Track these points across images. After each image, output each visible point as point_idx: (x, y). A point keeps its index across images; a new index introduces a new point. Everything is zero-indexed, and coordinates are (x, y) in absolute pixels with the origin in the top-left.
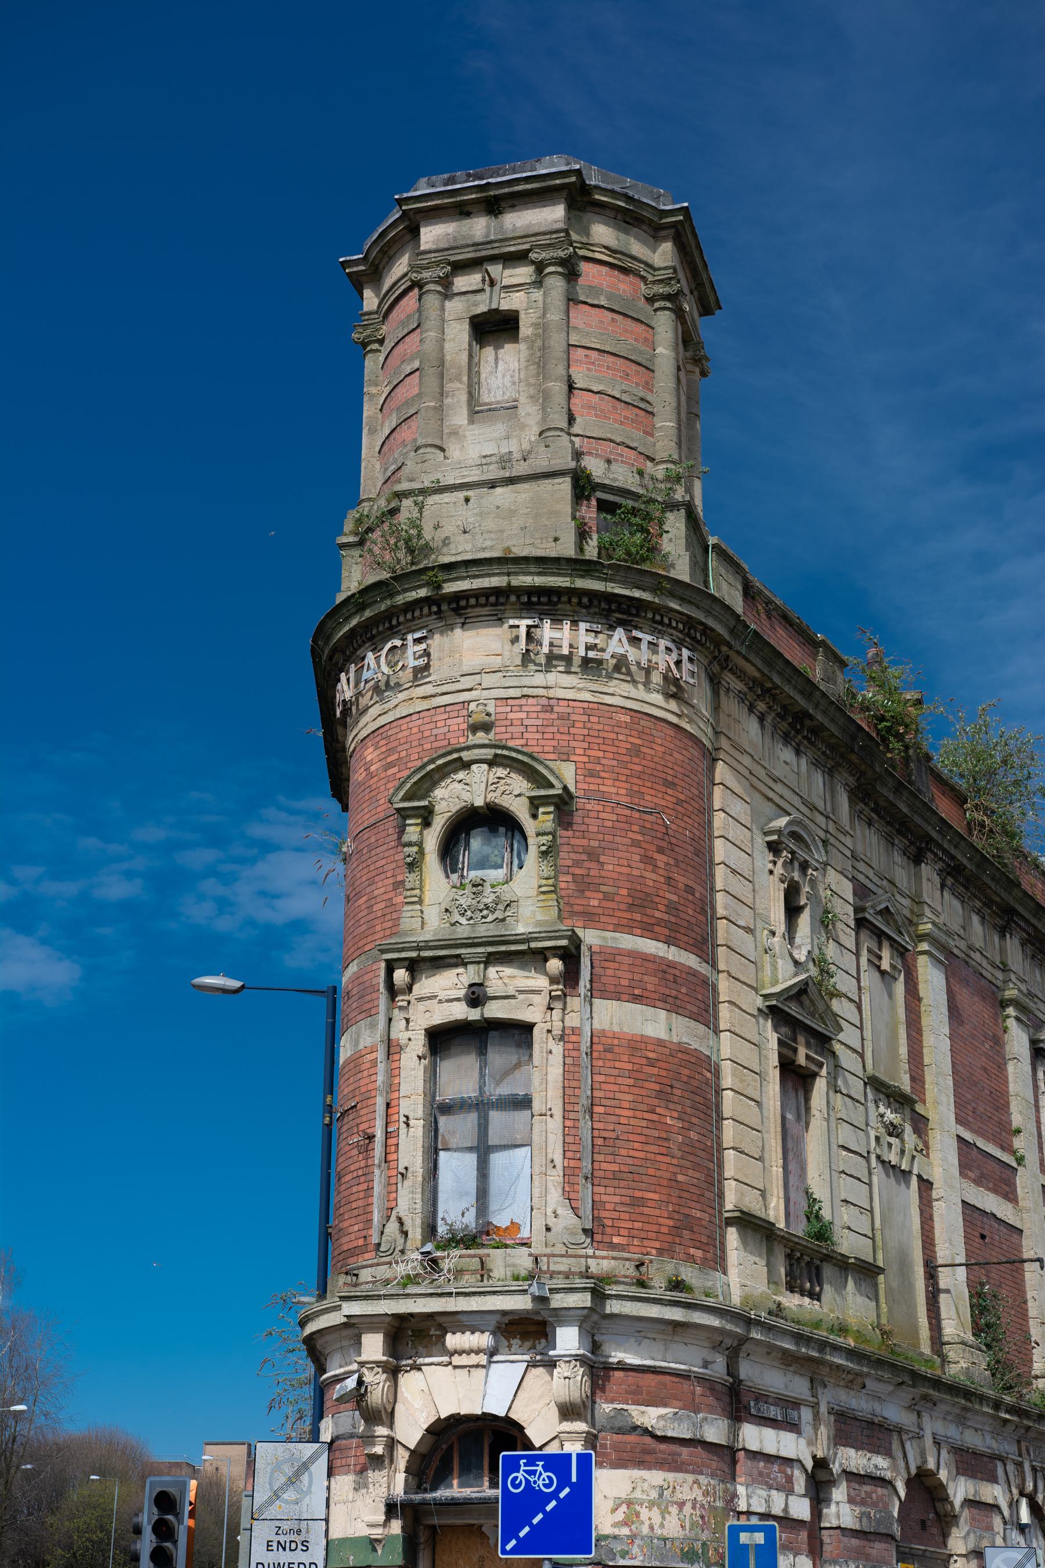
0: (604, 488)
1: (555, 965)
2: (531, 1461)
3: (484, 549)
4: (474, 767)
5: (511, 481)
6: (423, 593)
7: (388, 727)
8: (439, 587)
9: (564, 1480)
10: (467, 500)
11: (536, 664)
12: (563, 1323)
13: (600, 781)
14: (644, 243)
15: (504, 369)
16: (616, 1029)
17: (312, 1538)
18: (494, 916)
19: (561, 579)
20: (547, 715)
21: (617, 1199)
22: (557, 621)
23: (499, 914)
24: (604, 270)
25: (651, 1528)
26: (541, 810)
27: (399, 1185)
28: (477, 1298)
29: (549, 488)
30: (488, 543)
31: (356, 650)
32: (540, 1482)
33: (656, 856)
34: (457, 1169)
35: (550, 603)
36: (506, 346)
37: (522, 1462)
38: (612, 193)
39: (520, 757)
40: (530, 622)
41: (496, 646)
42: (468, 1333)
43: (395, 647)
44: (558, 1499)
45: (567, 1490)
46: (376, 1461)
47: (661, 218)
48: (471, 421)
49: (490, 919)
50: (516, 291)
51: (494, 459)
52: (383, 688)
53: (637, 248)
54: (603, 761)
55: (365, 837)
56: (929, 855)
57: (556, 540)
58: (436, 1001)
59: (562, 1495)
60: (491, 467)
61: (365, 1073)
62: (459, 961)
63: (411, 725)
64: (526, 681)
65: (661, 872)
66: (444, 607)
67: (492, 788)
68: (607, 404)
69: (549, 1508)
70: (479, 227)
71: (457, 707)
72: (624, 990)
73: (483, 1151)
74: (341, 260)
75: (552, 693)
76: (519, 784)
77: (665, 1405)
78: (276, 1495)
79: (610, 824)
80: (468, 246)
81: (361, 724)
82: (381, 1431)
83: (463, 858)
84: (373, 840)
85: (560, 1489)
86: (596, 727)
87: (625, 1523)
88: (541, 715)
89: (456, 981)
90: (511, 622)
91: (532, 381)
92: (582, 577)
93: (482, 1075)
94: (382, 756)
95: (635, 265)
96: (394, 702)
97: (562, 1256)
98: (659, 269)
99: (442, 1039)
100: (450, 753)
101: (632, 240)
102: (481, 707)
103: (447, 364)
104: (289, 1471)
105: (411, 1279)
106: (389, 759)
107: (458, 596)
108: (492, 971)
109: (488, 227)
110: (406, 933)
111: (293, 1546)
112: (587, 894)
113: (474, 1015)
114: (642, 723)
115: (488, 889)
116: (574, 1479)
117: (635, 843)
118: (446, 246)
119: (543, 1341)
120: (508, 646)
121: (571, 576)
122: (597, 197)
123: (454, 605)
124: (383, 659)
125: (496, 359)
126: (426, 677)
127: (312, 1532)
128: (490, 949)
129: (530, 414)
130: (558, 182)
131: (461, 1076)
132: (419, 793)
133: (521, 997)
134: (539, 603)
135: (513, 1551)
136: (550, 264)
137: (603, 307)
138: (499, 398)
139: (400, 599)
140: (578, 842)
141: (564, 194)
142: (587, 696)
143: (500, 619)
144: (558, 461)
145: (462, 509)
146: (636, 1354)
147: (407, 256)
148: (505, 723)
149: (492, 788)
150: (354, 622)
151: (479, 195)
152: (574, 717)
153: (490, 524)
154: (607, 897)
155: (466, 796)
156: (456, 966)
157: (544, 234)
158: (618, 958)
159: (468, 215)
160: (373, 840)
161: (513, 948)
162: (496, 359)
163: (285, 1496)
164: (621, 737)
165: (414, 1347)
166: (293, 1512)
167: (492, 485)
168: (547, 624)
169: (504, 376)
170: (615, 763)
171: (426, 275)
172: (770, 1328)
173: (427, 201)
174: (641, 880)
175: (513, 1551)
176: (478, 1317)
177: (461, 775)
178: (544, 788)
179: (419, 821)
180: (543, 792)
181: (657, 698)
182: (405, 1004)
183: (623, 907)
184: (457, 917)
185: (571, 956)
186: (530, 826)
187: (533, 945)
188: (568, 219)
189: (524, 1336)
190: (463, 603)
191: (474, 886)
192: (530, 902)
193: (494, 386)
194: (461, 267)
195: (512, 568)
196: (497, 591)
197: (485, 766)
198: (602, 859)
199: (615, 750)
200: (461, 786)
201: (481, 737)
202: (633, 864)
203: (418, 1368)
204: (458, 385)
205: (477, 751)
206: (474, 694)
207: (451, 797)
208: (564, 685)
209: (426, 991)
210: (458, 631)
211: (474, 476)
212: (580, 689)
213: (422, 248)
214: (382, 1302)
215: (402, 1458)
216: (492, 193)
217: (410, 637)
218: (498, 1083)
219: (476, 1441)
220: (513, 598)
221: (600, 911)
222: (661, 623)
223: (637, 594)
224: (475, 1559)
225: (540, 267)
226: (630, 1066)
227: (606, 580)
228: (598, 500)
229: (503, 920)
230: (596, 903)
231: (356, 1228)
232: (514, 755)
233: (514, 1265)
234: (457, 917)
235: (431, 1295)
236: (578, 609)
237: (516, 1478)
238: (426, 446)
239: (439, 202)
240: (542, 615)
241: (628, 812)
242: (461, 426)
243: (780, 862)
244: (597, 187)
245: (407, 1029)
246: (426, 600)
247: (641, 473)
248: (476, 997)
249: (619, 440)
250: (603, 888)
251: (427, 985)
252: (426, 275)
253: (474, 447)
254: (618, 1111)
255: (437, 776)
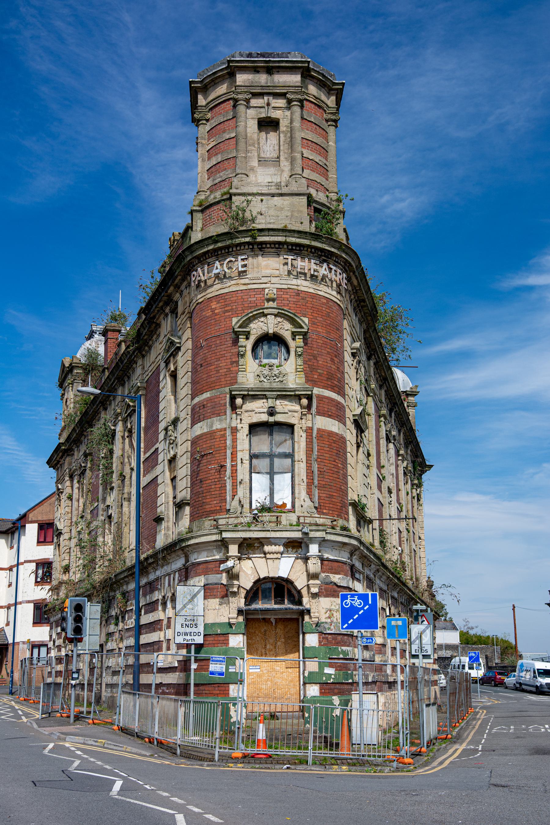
0: (316, 202)
1: (305, 402)
2: (353, 596)
3: (270, 223)
4: (268, 316)
5: (281, 195)
6: (248, 239)
7: (225, 295)
8: (256, 239)
9: (366, 603)
10: (262, 200)
11: (293, 275)
12: (312, 543)
13: (317, 326)
14: (325, 95)
15: (270, 143)
16: (323, 428)
17: (199, 623)
18: (279, 380)
19: (306, 241)
20: (297, 297)
21: (325, 495)
22: (303, 258)
23: (280, 379)
24: (313, 106)
25: (337, 619)
26: (297, 337)
27: (238, 486)
28: (279, 532)
29: (298, 200)
30: (272, 221)
31: (206, 259)
32: (357, 604)
33: (335, 358)
34: (260, 482)
35: (300, 250)
36: (271, 133)
37: (349, 596)
38: (318, 72)
39: (289, 314)
40: (292, 257)
41: (277, 266)
42: (273, 546)
43: (231, 261)
44: (364, 610)
45: (367, 607)
46: (234, 594)
47: (333, 86)
48: (259, 165)
49: (277, 380)
50: (277, 109)
51: (273, 184)
52: (223, 277)
53: (323, 97)
54: (318, 318)
55: (214, 340)
56: (373, 357)
57: (302, 223)
58: (254, 412)
59: (365, 608)
60: (272, 187)
61: (218, 440)
62: (265, 397)
63: (237, 295)
64: (290, 282)
65: (336, 365)
66: (255, 247)
67: (276, 326)
68: (315, 165)
69: (360, 613)
70: (262, 78)
71: (260, 290)
72: (326, 412)
73: (272, 474)
74: (190, 80)
75: (299, 288)
76: (287, 325)
77: (340, 574)
78: (185, 606)
79: (320, 344)
80: (258, 86)
81: (208, 291)
82: (236, 582)
83: (261, 353)
84: (218, 342)
85: (364, 606)
86: (315, 304)
87: (329, 617)
88: (295, 297)
89: (263, 405)
90: (285, 257)
91: (286, 151)
92: (314, 241)
93: (271, 444)
94: (222, 307)
95: (323, 105)
96: (229, 284)
97: (306, 517)
98: (331, 108)
99: (254, 428)
100: (259, 310)
101: (322, 94)
102: (271, 292)
103: (248, 138)
104: (189, 598)
105: (249, 524)
106: (226, 309)
107: (262, 243)
108: (278, 402)
109: (267, 79)
110: (242, 383)
111: (192, 626)
112: (313, 373)
113: (271, 419)
114: (330, 303)
115: (275, 368)
116: (370, 602)
117: (328, 353)
118: (249, 85)
119: (300, 549)
120: (282, 266)
121: (310, 240)
122: (312, 73)
123: (260, 247)
124: (225, 265)
125: (267, 138)
126: (245, 275)
127: (199, 620)
128: (279, 393)
129: (285, 164)
130: (300, 65)
131: (262, 443)
132: (244, 325)
133: (290, 413)
134: (296, 250)
135: (346, 628)
136: (295, 101)
137: (312, 122)
138: (268, 156)
139: (238, 241)
140: (309, 351)
141: (301, 70)
142: (311, 291)
143: (278, 254)
144: (302, 189)
145: (259, 204)
146: (331, 555)
147: (226, 84)
148: (281, 299)
149: (276, 326)
150: (211, 247)
151: (265, 65)
152: (308, 299)
153: (272, 212)
154: (320, 375)
155: (265, 328)
156: (263, 399)
157: (292, 87)
158: (324, 400)
159: (258, 72)
160: (218, 342)
161: (288, 393)
162: (267, 138)
163: (188, 607)
164: (324, 309)
165: (247, 550)
166: (191, 613)
167: (273, 195)
168: (299, 259)
169: (270, 146)
170: (321, 319)
171: (240, 96)
172: (368, 548)
173: (241, 63)
174: (330, 368)
175: (346, 628)
176: (278, 540)
177: (262, 319)
178: (297, 328)
179: (245, 337)
180: (299, 330)
181: (334, 293)
182: (240, 413)
183: (325, 379)
184: (262, 379)
185: (310, 398)
186: (292, 344)
187: (297, 393)
188: (302, 81)
189: (293, 547)
190: (264, 246)
191: (270, 366)
192: (292, 375)
193: (266, 150)
194: (256, 95)
195: (288, 234)
196: (279, 243)
197: (273, 317)
198: (318, 359)
199: (322, 314)
200: (262, 324)
201: (271, 304)
202: (328, 362)
203: (250, 559)
204: (253, 148)
205: (271, 310)
206: (267, 286)
207: (257, 328)
208: (305, 285)
209: (249, 408)
210: (260, 258)
211: (265, 190)
212: (310, 288)
213: (237, 84)
214: (240, 533)
215: (243, 593)
216: (271, 65)
217: (240, 258)
218: (278, 447)
219: (281, 588)
220: (285, 246)
221: (318, 380)
222: (337, 262)
223: (333, 250)
224: (262, 631)
225: (289, 101)
226: (328, 443)
227: (322, 243)
228: (314, 207)
229: (282, 381)
230: (316, 377)
231: (215, 502)
232: (287, 313)
233: (290, 520)
234: (262, 379)
235: (260, 531)
236: (310, 253)
237: (346, 602)
238: (242, 174)
239: (247, 64)
240: (297, 254)
241: (326, 340)
242: (255, 167)
243: (355, 361)
244: (313, 69)
245: (241, 423)
246: (248, 243)
247: (327, 197)
248: (272, 412)
249: (318, 181)
250: (319, 371)
251: (249, 405)
252: (240, 96)
253: (262, 178)
254: (324, 461)
255: (252, 319)
